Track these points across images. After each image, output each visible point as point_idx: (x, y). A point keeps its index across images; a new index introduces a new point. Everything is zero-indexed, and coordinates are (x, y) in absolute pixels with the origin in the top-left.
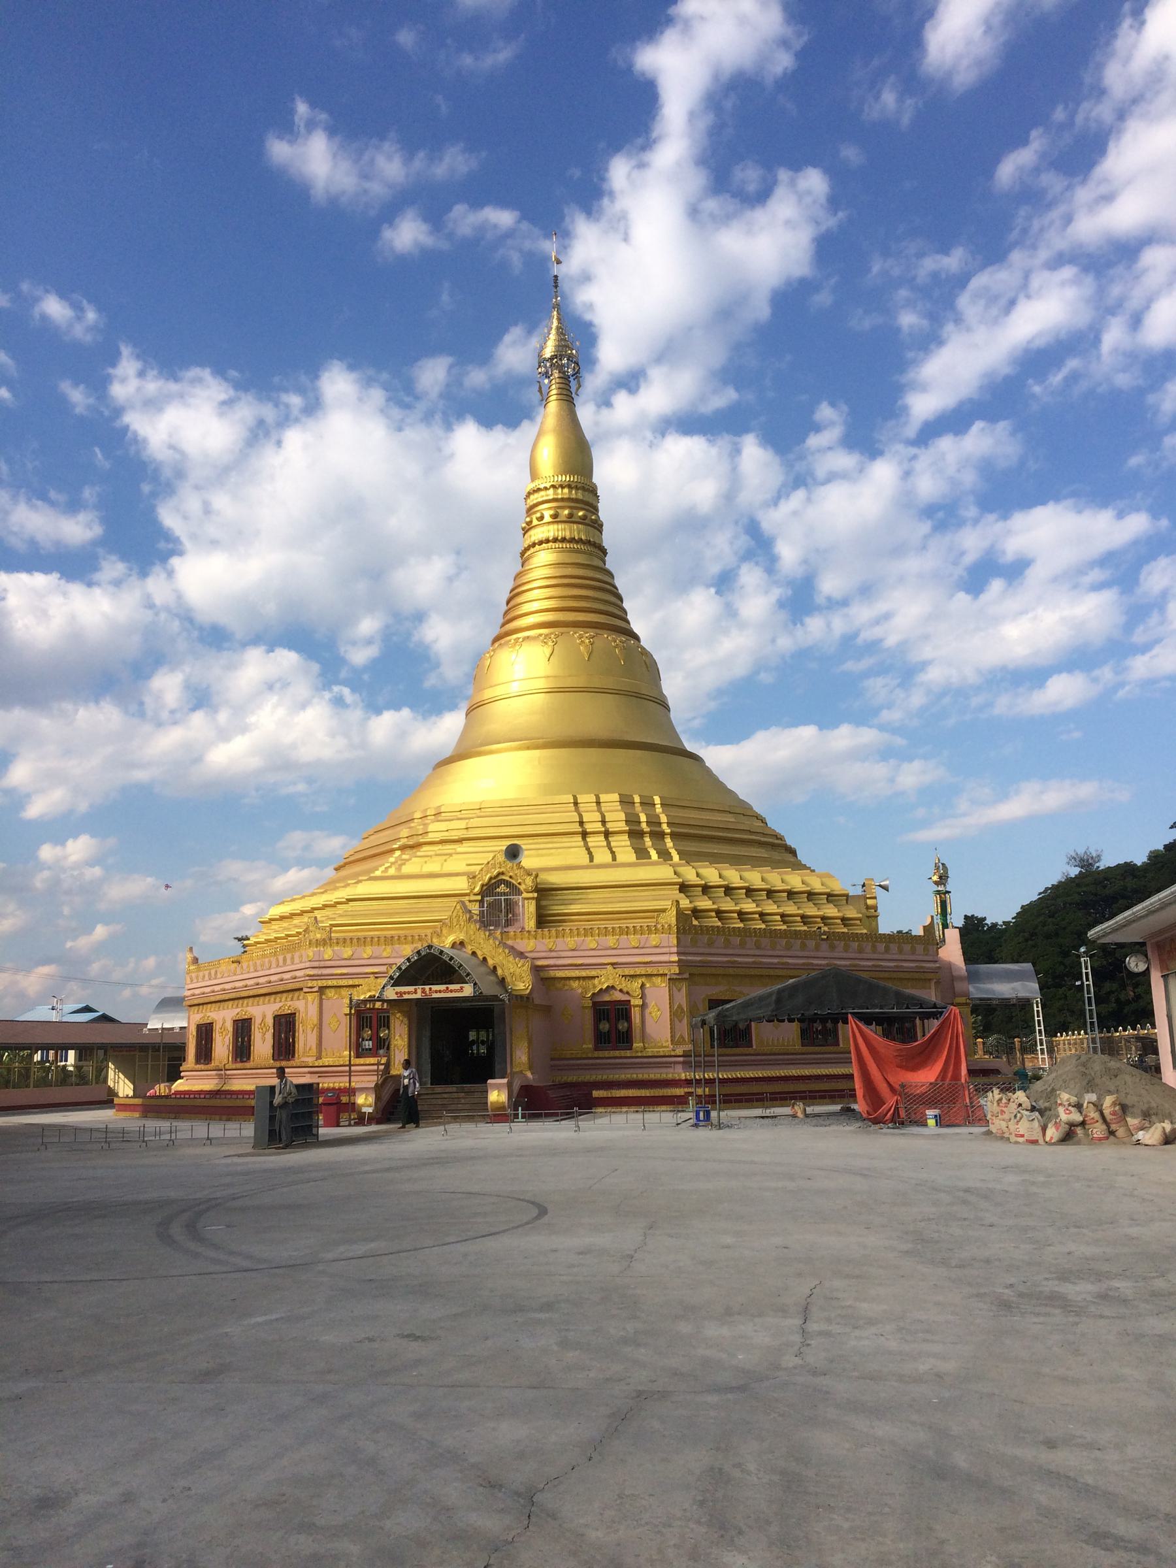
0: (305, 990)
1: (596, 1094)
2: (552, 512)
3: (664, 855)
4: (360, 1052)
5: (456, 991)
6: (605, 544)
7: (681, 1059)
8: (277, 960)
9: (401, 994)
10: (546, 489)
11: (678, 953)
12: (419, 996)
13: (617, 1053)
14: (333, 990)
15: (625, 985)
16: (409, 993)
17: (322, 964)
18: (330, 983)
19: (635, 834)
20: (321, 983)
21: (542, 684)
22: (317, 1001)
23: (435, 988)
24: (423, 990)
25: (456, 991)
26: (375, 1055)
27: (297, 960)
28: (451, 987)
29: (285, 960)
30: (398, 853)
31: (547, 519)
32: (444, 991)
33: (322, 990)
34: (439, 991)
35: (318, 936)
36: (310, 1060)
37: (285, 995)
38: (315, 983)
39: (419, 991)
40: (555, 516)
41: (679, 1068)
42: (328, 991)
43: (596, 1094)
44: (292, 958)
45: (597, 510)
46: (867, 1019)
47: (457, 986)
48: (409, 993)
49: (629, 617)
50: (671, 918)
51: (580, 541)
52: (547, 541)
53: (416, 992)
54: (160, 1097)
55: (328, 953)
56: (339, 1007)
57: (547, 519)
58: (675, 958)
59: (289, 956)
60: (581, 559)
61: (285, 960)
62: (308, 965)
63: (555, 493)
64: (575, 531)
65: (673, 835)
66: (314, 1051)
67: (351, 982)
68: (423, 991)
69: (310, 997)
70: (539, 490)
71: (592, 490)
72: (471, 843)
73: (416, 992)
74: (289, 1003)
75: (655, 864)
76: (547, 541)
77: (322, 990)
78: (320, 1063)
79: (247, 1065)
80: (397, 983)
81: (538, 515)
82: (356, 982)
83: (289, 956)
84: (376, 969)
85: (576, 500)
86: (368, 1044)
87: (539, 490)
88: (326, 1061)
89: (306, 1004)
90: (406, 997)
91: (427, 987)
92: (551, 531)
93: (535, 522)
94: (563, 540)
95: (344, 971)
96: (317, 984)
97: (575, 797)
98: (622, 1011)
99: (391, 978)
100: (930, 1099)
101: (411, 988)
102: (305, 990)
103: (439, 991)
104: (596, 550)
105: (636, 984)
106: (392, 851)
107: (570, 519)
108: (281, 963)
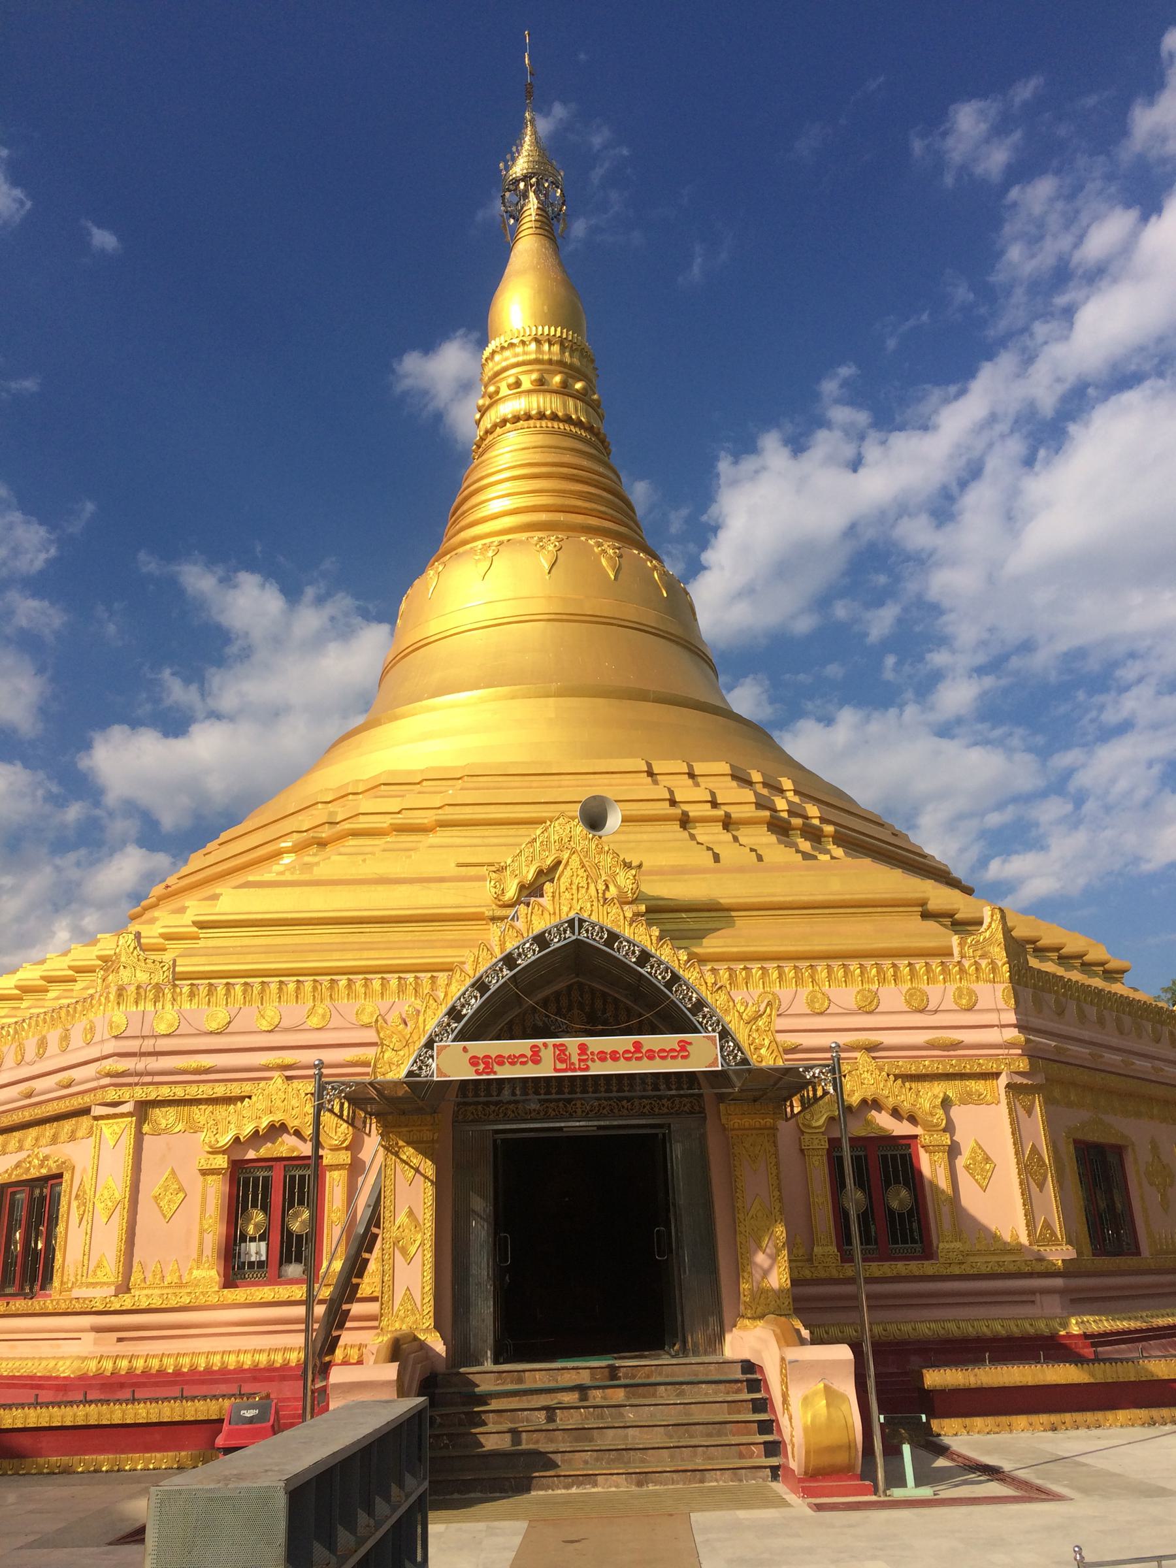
0: (98, 1111)
1: (934, 1378)
2: (534, 376)
4: (235, 1270)
5: (664, 1054)
7: (1059, 1282)
8: (21, 1048)
9: (489, 1062)
11: (1021, 1027)
12: (546, 1069)
13: (901, 1267)
14: (171, 1111)
15: (904, 1096)
16: (513, 1060)
17: (148, 1045)
18: (165, 1092)
20: (140, 1093)
21: (538, 607)
22: (128, 1140)
23: (596, 1043)
24: (562, 1049)
25: (664, 1054)
26: (278, 1279)
27: (77, 1038)
28: (650, 1041)
29: (42, 1044)
30: (288, 859)
32: (628, 1056)
33: (143, 1109)
34: (610, 1055)
35: (142, 977)
36: (99, 1295)
37: (33, 1132)
38: (126, 1094)
39: (547, 1055)
40: (541, 382)
41: (1053, 1306)
42: (157, 1113)
43: (934, 1378)
44: (65, 1038)
47: (669, 1040)
48: (513, 1060)
51: (579, 424)
52: (528, 417)
53: (536, 1058)
55: (165, 1017)
56: (190, 1160)
58: (1012, 1034)
59: (53, 1036)
60: (568, 458)
61: (42, 1044)
62: (111, 1047)
63: (539, 351)
66: (110, 1271)
67: (220, 1090)
68: (561, 1055)
69: (109, 1130)
72: (455, 831)
73: (536, 1058)
74: (44, 1151)
76: (528, 417)
77: (143, 1109)
78: (127, 1302)
79: (36, 1305)
80: (475, 1029)
81: (512, 380)
82: (235, 1089)
83: (53, 1036)
84: (289, 1057)
85: (571, 367)
86: (256, 1251)
88: (141, 1297)
89: (99, 1146)
90: (504, 1072)
91: (572, 1043)
92: (533, 403)
93: (504, 391)
94: (554, 417)
96: (133, 1095)
97: (649, 765)
98: (891, 1162)
99: (454, 1013)
101: (522, 1046)
102: (98, 1111)
103: (610, 1055)
105: (928, 1096)
106: (279, 854)
107: (565, 390)
108: (30, 1054)
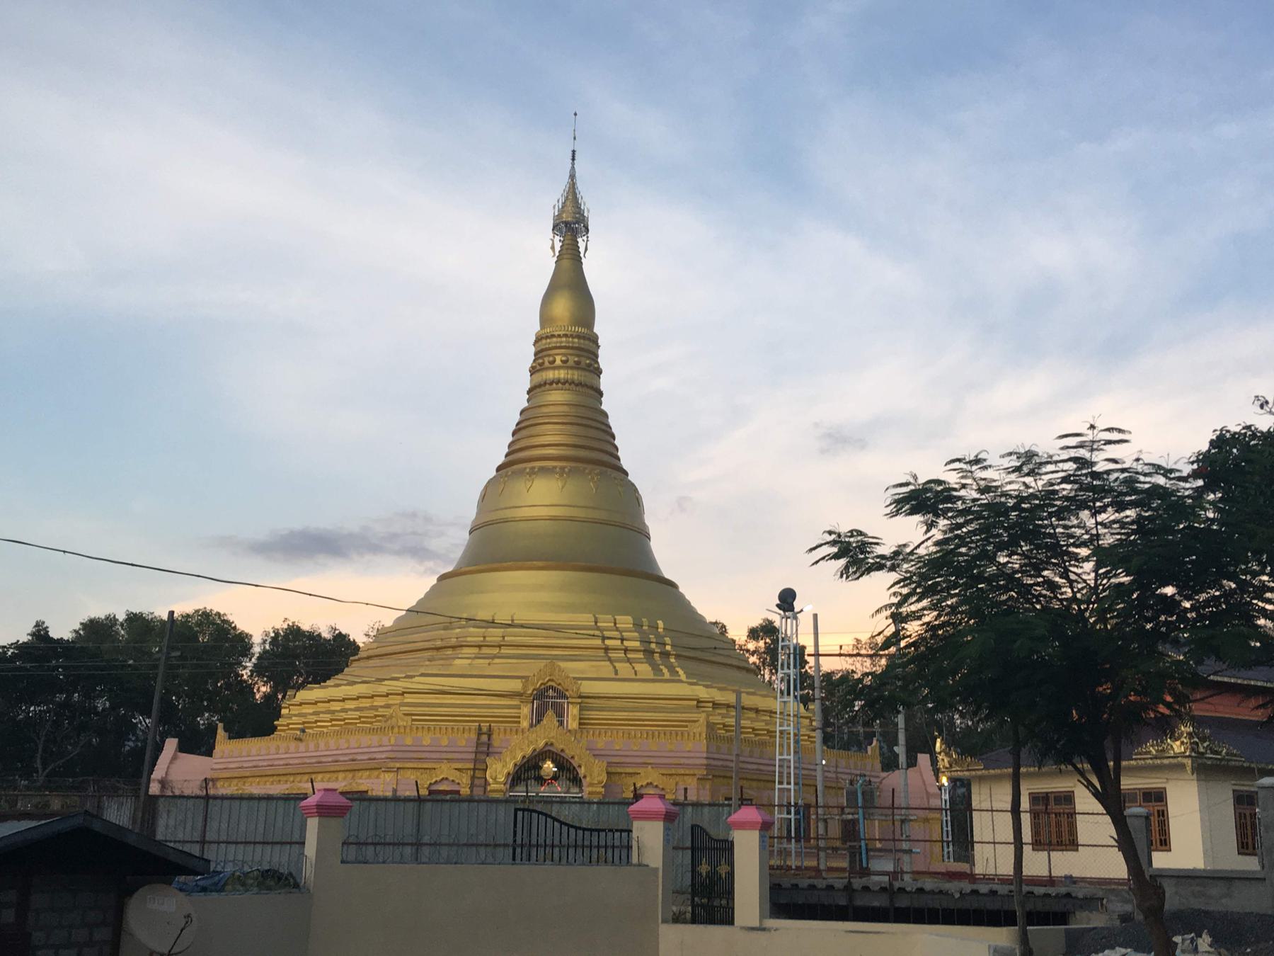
3: (672, 669)
6: (602, 388)
10: (559, 336)
19: (649, 653)
20: (398, 765)
31: (558, 362)
45: (597, 356)
46: (1076, 898)
49: (619, 454)
50: (700, 729)
54: (190, 855)
57: (558, 362)
64: (575, 375)
65: (677, 656)
70: (553, 336)
71: (594, 340)
75: (681, 681)
87: (553, 336)
93: (547, 364)
95: (415, 755)
100: (227, 640)
104: (592, 392)
